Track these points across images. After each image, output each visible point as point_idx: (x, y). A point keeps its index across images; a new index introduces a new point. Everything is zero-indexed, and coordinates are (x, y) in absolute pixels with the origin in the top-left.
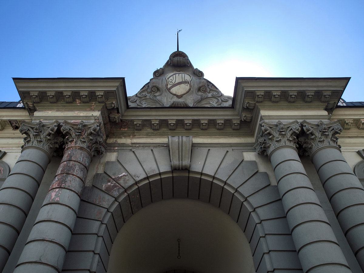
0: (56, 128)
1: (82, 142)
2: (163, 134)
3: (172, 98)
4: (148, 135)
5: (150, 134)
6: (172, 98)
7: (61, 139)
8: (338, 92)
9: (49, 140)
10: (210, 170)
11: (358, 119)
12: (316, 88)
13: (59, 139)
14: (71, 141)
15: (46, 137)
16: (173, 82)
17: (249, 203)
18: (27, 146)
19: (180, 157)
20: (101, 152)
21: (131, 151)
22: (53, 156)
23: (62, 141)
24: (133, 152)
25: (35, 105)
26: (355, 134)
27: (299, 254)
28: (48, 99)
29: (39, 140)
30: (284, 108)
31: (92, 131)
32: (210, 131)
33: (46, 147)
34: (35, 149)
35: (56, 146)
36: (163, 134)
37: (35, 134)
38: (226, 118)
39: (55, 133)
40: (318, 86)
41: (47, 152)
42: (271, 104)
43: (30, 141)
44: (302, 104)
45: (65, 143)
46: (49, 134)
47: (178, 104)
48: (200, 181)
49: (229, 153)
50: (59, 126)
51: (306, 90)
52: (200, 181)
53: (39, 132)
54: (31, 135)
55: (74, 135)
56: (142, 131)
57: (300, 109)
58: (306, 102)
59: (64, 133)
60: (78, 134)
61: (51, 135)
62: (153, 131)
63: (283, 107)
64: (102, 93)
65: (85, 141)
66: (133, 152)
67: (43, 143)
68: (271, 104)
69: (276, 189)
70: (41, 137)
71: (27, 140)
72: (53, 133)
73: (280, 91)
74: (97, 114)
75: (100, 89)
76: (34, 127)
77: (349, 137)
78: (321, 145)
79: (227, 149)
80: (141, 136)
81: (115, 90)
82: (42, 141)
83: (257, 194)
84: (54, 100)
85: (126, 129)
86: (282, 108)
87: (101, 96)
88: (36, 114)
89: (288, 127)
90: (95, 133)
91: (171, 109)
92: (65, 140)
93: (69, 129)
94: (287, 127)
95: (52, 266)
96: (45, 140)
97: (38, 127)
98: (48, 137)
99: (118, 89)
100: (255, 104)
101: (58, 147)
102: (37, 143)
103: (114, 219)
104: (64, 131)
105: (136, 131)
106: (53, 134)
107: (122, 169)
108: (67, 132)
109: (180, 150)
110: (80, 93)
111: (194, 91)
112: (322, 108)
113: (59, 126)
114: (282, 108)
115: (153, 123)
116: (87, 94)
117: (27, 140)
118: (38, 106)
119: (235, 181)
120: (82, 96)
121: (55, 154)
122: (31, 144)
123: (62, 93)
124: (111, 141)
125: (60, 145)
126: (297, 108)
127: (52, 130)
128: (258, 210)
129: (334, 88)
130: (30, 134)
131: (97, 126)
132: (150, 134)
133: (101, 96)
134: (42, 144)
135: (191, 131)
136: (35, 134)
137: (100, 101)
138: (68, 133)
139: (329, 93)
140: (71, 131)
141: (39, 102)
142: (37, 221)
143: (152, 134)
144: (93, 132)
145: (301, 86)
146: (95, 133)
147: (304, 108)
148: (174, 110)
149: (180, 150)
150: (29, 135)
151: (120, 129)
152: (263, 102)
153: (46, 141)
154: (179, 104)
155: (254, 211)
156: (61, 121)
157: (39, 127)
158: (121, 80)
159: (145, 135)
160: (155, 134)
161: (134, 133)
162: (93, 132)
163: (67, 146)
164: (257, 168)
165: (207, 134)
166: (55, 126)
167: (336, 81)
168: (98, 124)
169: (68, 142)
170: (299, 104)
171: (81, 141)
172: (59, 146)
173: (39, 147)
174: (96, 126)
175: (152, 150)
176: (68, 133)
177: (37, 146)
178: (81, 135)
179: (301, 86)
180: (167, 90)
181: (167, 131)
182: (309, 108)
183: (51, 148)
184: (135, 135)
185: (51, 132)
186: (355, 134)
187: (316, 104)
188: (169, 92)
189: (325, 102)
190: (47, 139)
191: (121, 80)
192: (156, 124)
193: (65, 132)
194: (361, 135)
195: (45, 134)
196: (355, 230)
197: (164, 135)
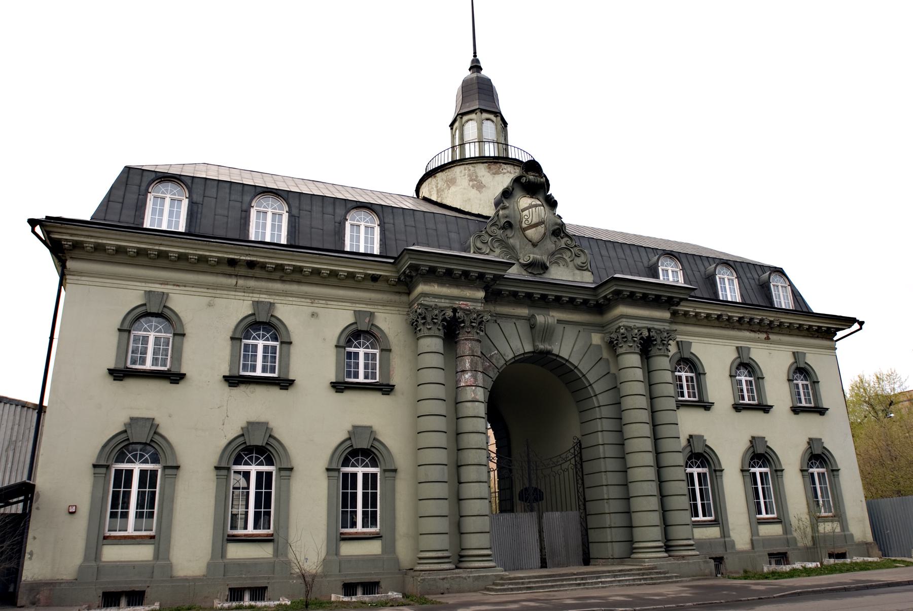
3: (527, 244)
6: (527, 244)
10: (565, 354)
16: (530, 220)
17: (592, 388)
19: (543, 338)
21: (496, 322)
24: (498, 324)
27: (143, 320)
47: (539, 262)
48: (585, 388)
49: (581, 333)
52: (585, 388)
66: (498, 324)
69: (615, 377)
78: (658, 353)
83: (599, 381)
89: (442, 311)
107: (493, 348)
111: (548, 236)
119: (584, 367)
128: (600, 397)
155: (596, 395)
164: (602, 354)
175: (515, 323)
180: (520, 230)
184: (497, 301)
188: (523, 232)
196: (669, 497)
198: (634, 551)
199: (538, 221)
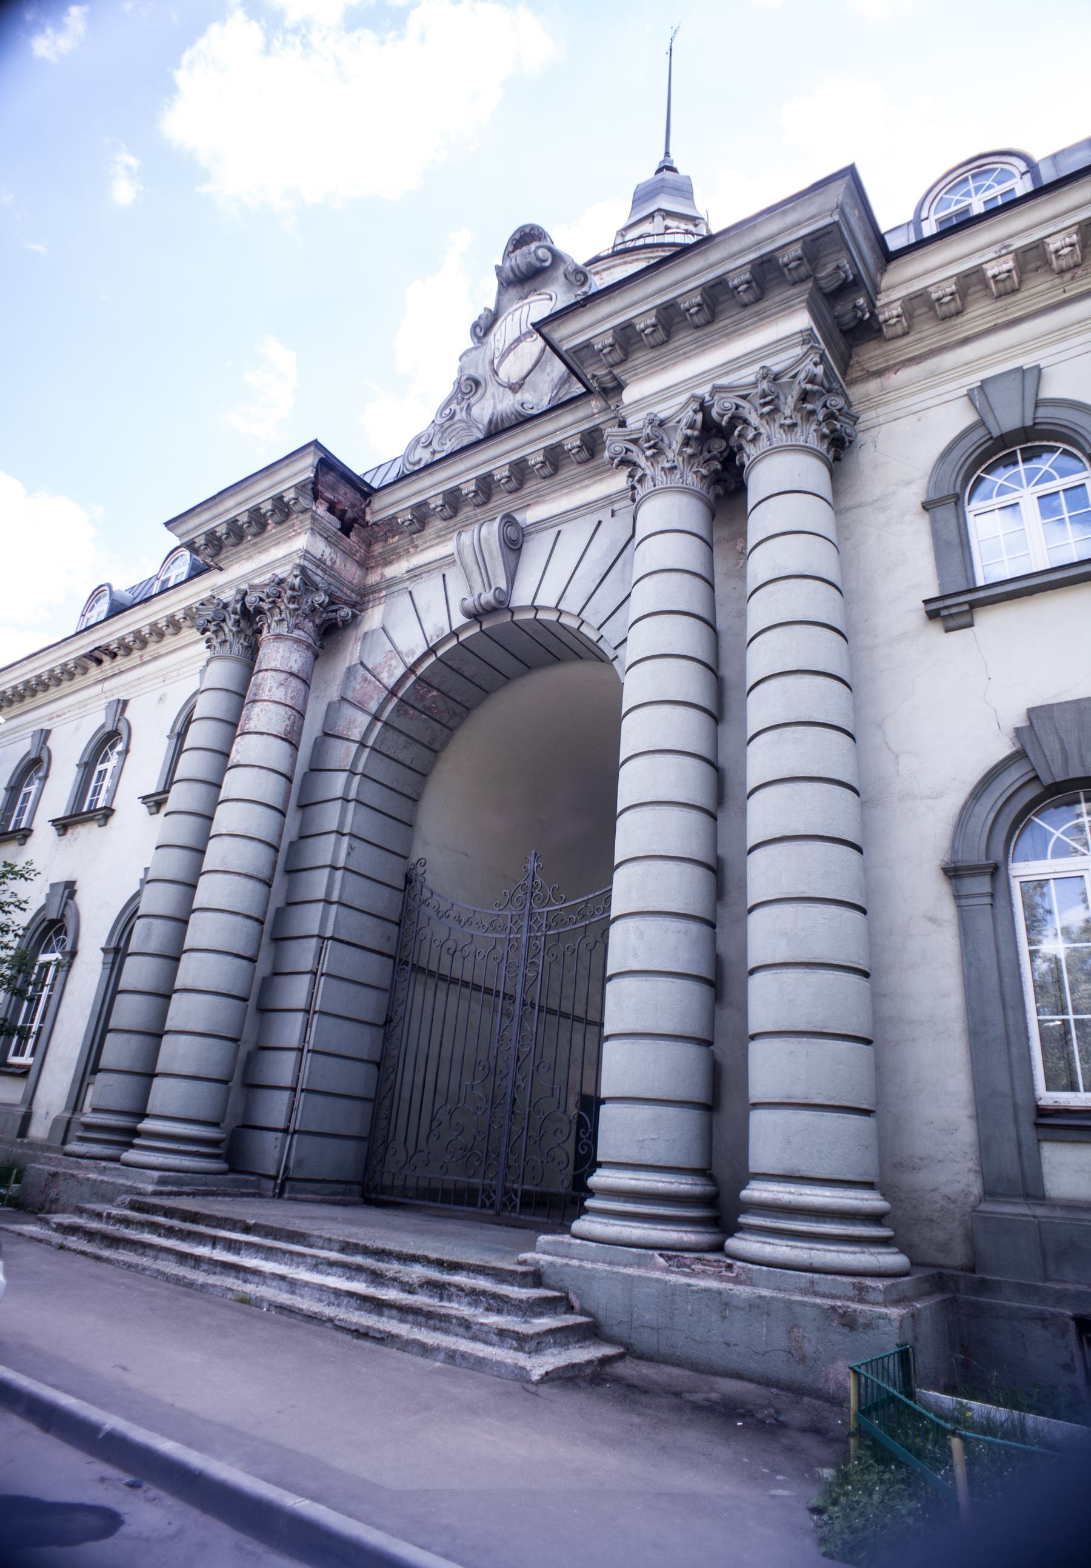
0: (699, 417)
1: (786, 428)
2: (468, 522)
4: (440, 536)
5: (443, 533)
7: (718, 445)
8: (829, 233)
9: (691, 456)
11: (1038, 243)
12: (755, 251)
13: (716, 446)
14: (754, 440)
15: (680, 453)
18: (645, 493)
20: (846, 440)
22: (717, 497)
23: (723, 448)
25: (615, 372)
26: (985, 320)
28: (642, 340)
29: (667, 465)
30: (690, 351)
31: (685, 432)
32: (568, 474)
33: (692, 480)
34: (661, 495)
35: (712, 468)
36: (468, 522)
37: (649, 453)
38: (582, 428)
39: (700, 432)
40: (759, 243)
41: (821, 453)
42: (652, 354)
43: (644, 475)
44: (736, 318)
45: (735, 449)
46: (687, 440)
47: (502, 421)
50: (704, 408)
51: (724, 274)
53: (772, 400)
54: (642, 461)
55: (754, 419)
56: (426, 532)
57: (737, 334)
58: (745, 306)
59: (723, 423)
60: (767, 409)
61: (692, 443)
62: (445, 523)
63: (685, 350)
64: (745, 274)
65: (794, 421)
67: (679, 473)
68: (651, 355)
70: (667, 457)
71: (637, 478)
72: (696, 433)
73: (654, 311)
74: (801, 320)
75: (287, 482)
76: (640, 435)
77: (965, 341)
79: (595, 518)
80: (428, 544)
81: (835, 223)
82: (675, 468)
84: (660, 335)
85: (397, 537)
86: (685, 353)
87: (798, 262)
88: (629, 395)
90: (816, 387)
91: (457, 458)
92: (733, 441)
93: (734, 407)
94: (790, 378)
95: (247, 876)
96: (683, 462)
97: (648, 431)
98: (689, 451)
99: (843, 214)
100: (611, 372)
101: (719, 467)
102: (664, 477)
103: (386, 756)
104: (722, 416)
105: (414, 536)
106: (697, 438)
108: (732, 418)
109: (481, 563)
110: (777, 260)
112: (800, 303)
113: (704, 408)
114: (685, 353)
115: (934, 296)
116: (699, 298)
117: (637, 478)
118: (625, 372)
120: (688, 310)
121: (720, 490)
122: (768, 443)
123: (588, 346)
124: (373, 578)
125: (722, 459)
126: (727, 335)
127: (691, 426)
129: (809, 225)
130: (748, 417)
131: (695, 412)
132: (443, 533)
133: (798, 262)
134: (678, 476)
135: (966, 317)
136: (649, 453)
137: (653, 343)
138: (737, 419)
139: (796, 251)
140: (632, 452)
141: (623, 358)
142: (749, 685)
143: (448, 531)
144: (809, 386)
145: (711, 266)
146: (816, 387)
147: (747, 326)
148: (463, 455)
149: (481, 563)
150: (635, 464)
151: (386, 541)
152: (629, 360)
153: (686, 463)
154: (504, 416)
156: (704, 390)
157: (652, 431)
158: (312, 448)
159: (435, 539)
160: (452, 529)
161: (412, 541)
162: (809, 386)
163: (748, 456)
165: (560, 486)
166: (695, 412)
167: (810, 198)
168: (817, 359)
169: (744, 442)
170: (728, 321)
171: (782, 426)
172: (720, 463)
173: (673, 485)
174: (691, 413)
176: (737, 419)
177: (669, 485)
178: (776, 410)
179: (711, 266)
181: (474, 512)
182: (762, 320)
183: (704, 477)
185: (689, 432)
186: (985, 320)
187: (778, 298)
189: (802, 280)
190: (686, 456)
191: (312, 448)
192: (946, 296)
193: (726, 418)
194: (1007, 315)
195: (789, 398)
197: (471, 523)
198: (137, 1141)
199: (518, 334)
